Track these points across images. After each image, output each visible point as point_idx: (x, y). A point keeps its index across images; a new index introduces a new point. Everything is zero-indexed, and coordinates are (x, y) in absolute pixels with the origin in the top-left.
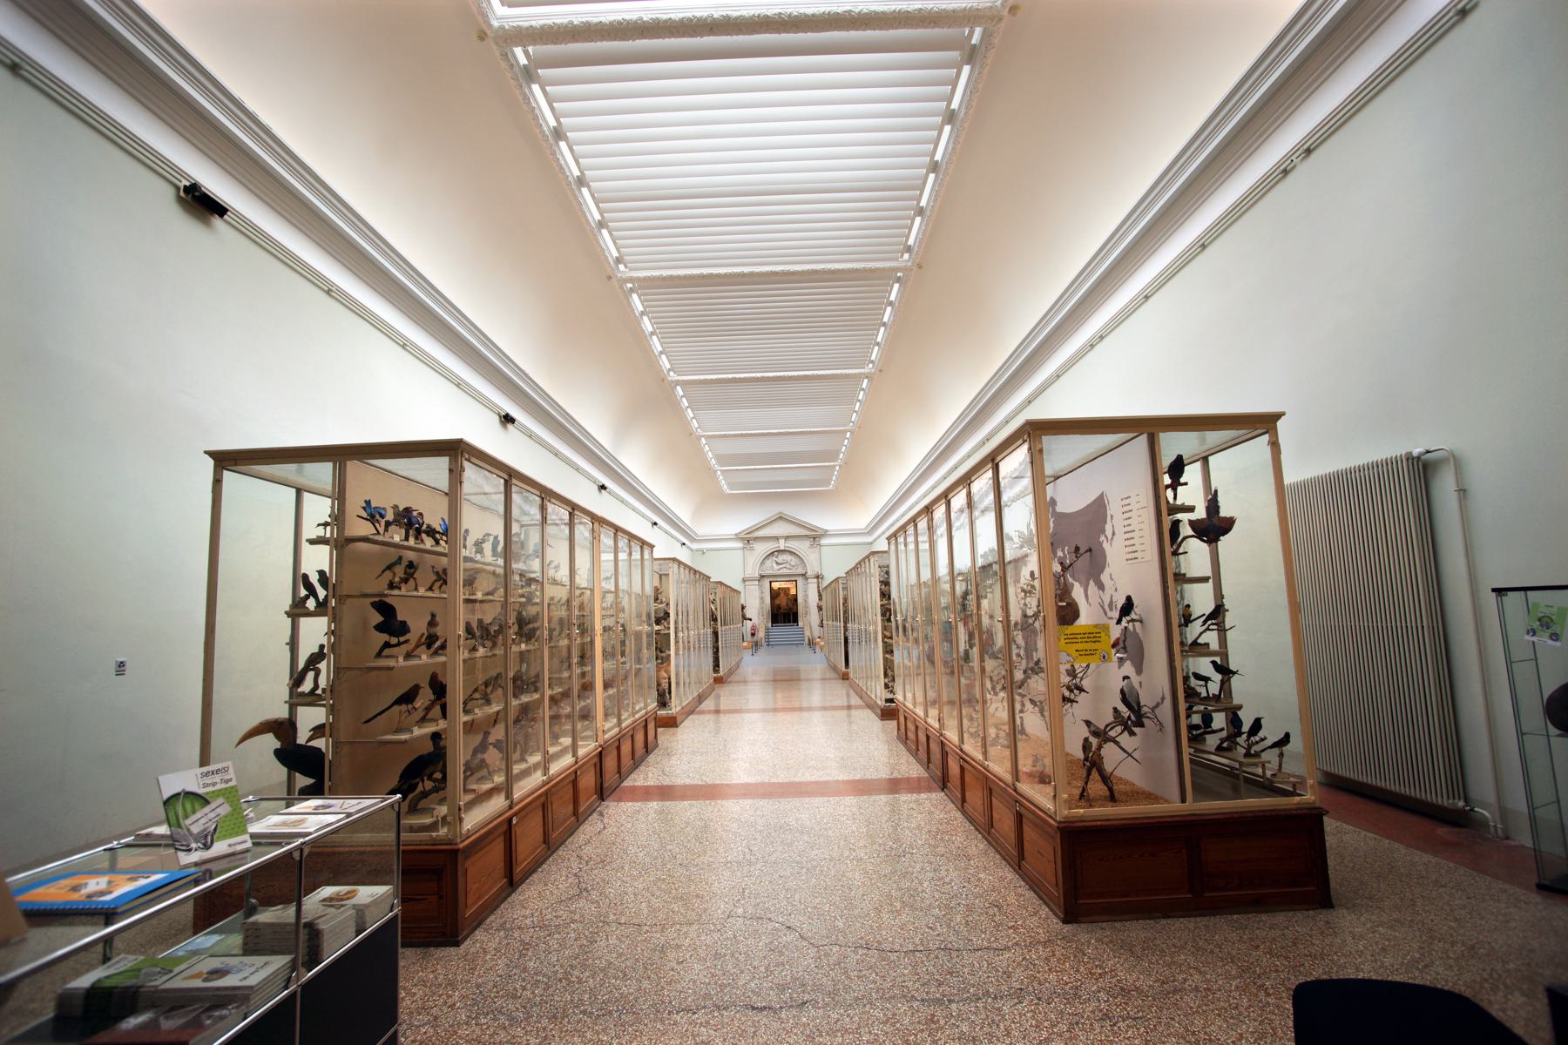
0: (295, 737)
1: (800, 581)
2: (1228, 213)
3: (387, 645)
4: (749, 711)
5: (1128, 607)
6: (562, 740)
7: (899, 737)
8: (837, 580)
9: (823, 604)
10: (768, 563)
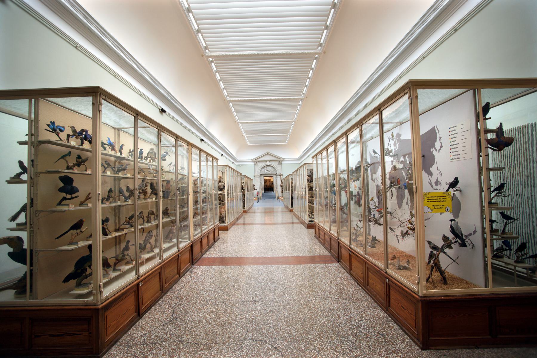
0: (23, 246)
1: (274, 176)
2: (472, 12)
3: (65, 199)
4: (255, 224)
5: (454, 184)
6: (173, 240)
7: (315, 236)
8: (288, 176)
9: (283, 185)
10: (263, 170)
